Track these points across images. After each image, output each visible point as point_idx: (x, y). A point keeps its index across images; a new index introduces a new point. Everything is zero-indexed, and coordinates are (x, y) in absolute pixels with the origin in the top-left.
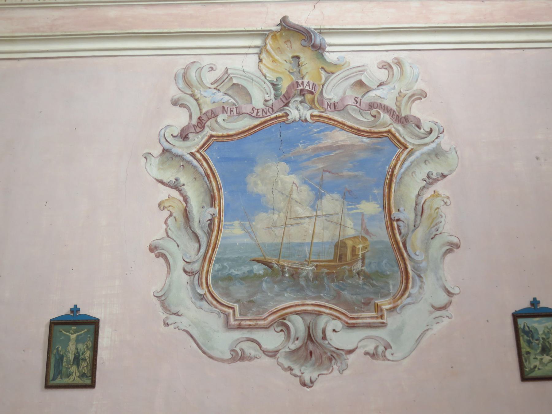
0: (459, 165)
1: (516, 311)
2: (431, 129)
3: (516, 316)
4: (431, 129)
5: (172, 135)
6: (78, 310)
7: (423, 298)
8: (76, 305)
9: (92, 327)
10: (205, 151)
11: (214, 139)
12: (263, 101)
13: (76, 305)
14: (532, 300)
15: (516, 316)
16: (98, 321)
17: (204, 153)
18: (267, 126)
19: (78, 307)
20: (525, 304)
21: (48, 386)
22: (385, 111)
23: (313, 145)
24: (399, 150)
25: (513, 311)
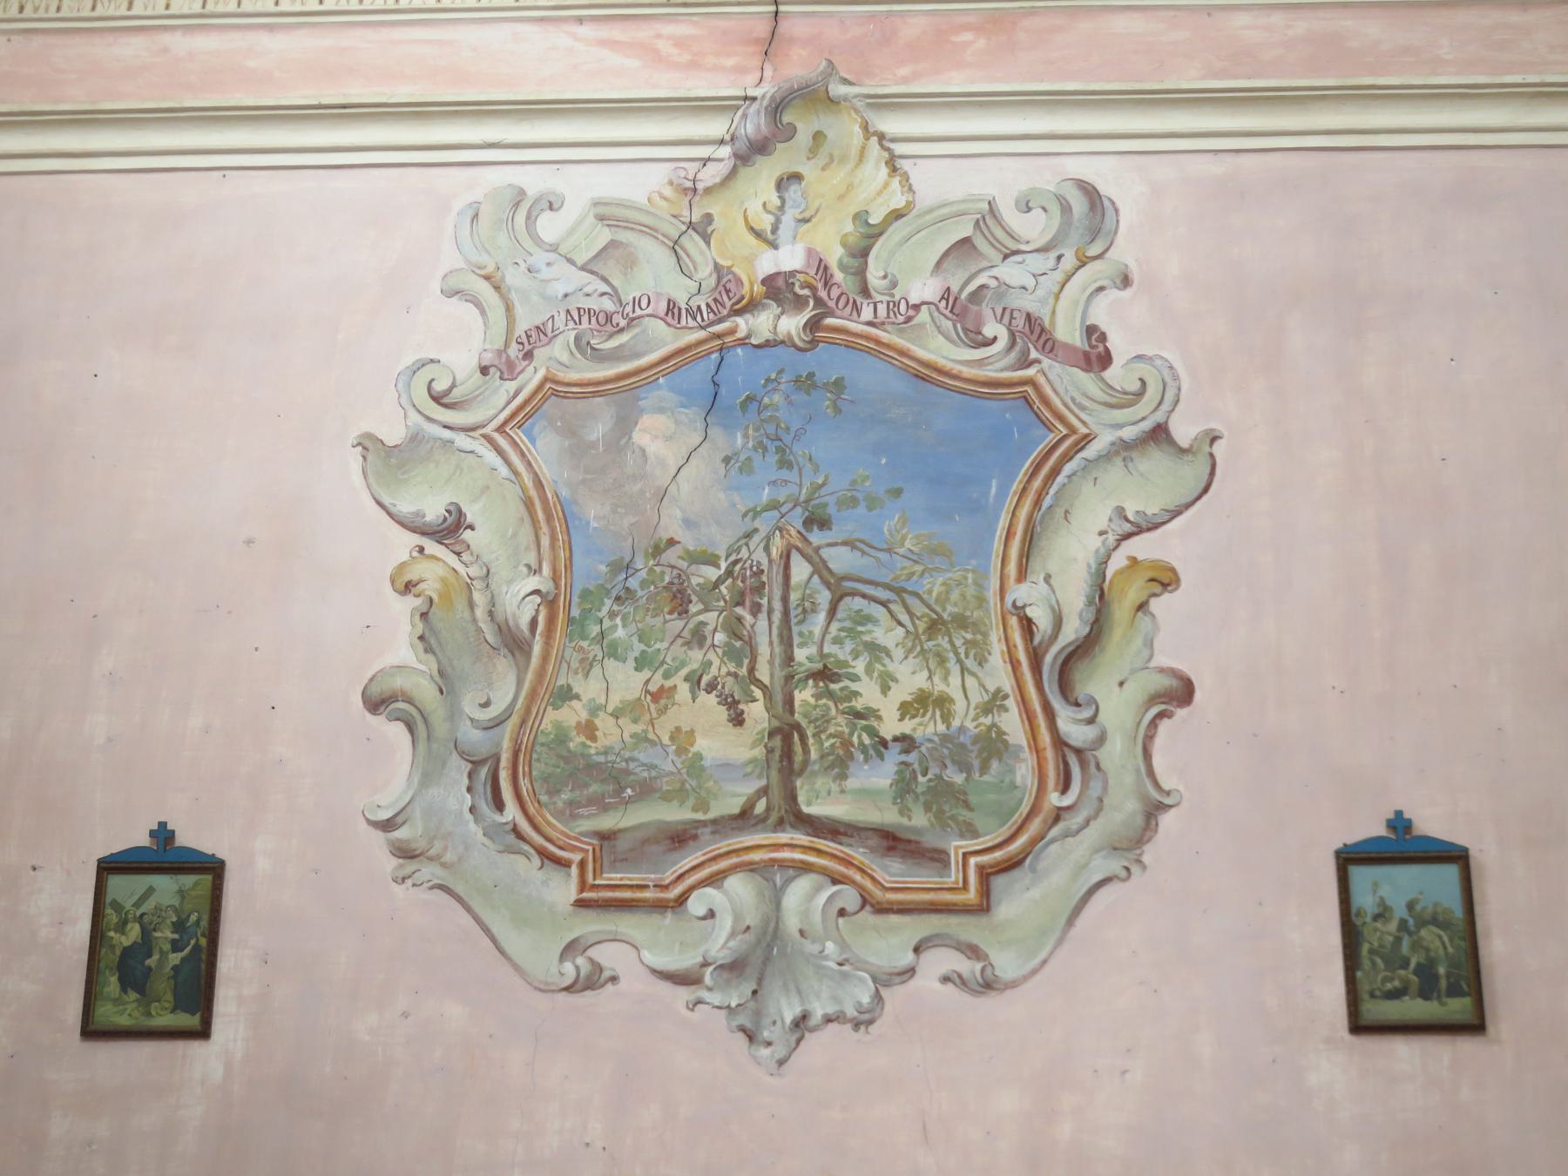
0: (953, 333)
1: (1345, 845)
2: (1141, 379)
3: (1347, 859)
4: (1141, 379)
5: (433, 380)
6: (170, 836)
7: (800, 210)
8: (166, 823)
9: (207, 879)
10: (519, 428)
11: (553, 389)
12: (538, 322)
13: (166, 823)
14: (1391, 816)
15: (1347, 859)
16: (221, 864)
17: (517, 434)
18: (693, 358)
19: (169, 828)
20: (1372, 827)
21: (92, 1031)
22: (656, 198)
23: (799, 742)
24: (1052, 436)
25: (1338, 845)
